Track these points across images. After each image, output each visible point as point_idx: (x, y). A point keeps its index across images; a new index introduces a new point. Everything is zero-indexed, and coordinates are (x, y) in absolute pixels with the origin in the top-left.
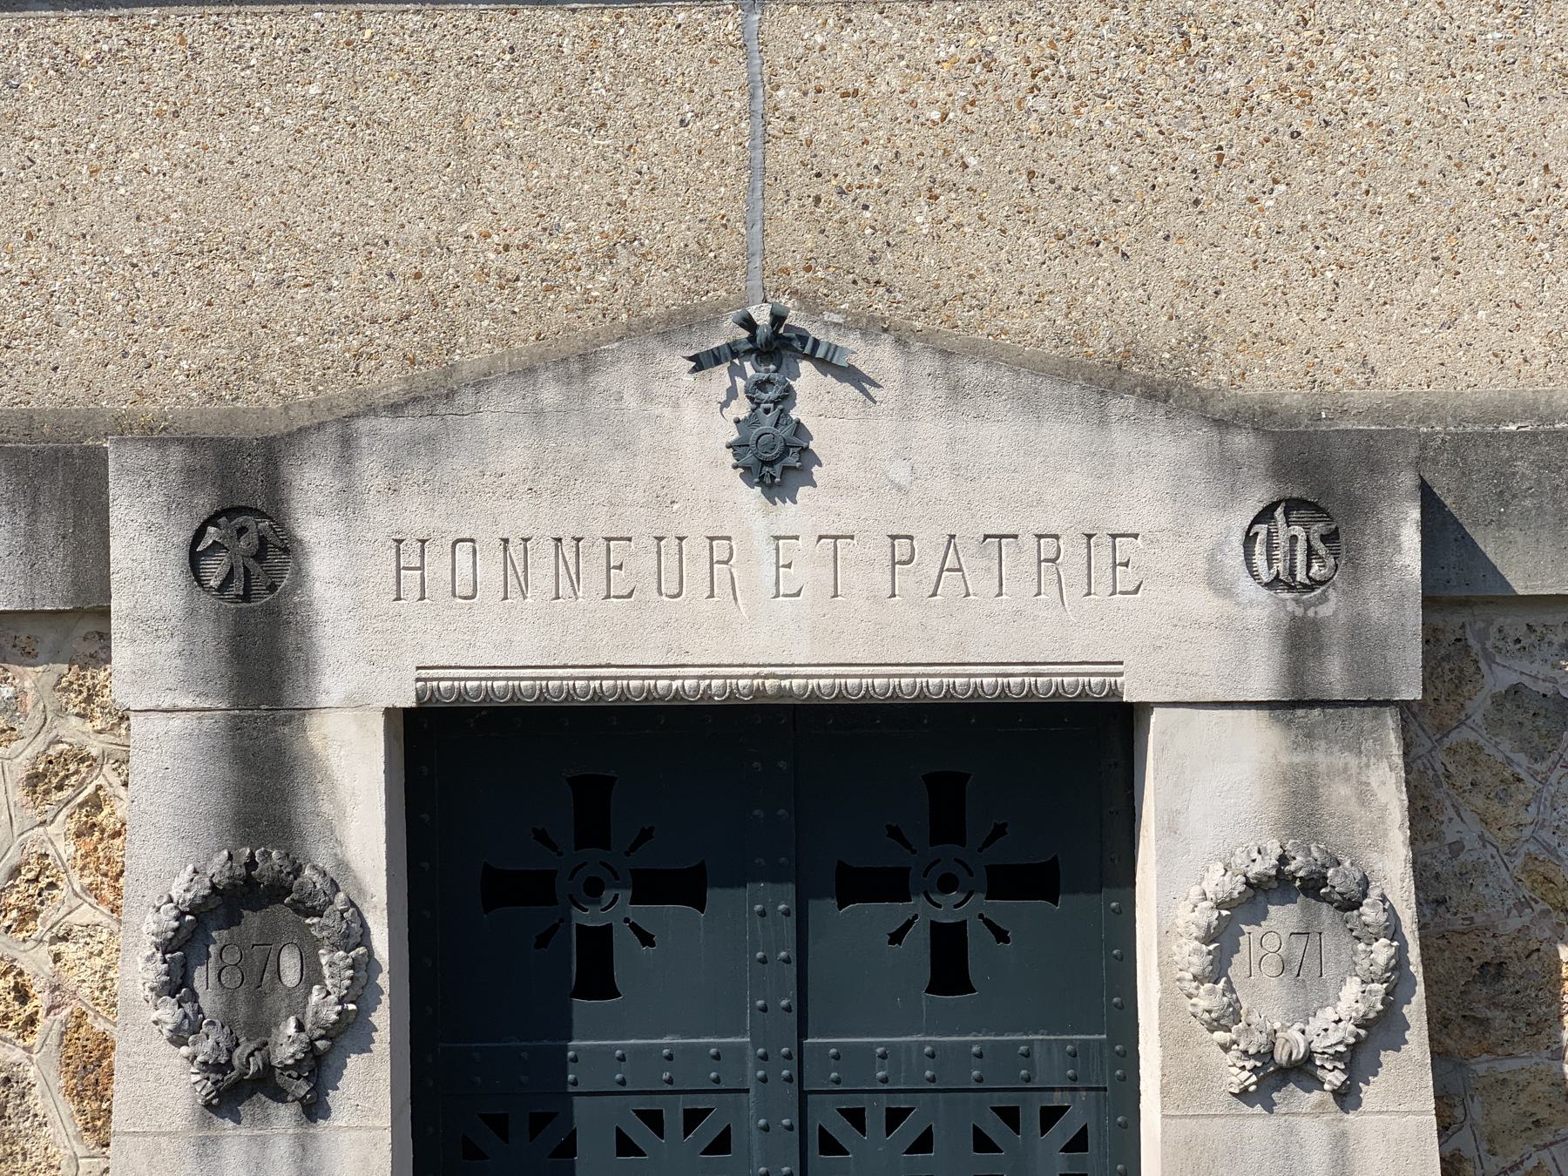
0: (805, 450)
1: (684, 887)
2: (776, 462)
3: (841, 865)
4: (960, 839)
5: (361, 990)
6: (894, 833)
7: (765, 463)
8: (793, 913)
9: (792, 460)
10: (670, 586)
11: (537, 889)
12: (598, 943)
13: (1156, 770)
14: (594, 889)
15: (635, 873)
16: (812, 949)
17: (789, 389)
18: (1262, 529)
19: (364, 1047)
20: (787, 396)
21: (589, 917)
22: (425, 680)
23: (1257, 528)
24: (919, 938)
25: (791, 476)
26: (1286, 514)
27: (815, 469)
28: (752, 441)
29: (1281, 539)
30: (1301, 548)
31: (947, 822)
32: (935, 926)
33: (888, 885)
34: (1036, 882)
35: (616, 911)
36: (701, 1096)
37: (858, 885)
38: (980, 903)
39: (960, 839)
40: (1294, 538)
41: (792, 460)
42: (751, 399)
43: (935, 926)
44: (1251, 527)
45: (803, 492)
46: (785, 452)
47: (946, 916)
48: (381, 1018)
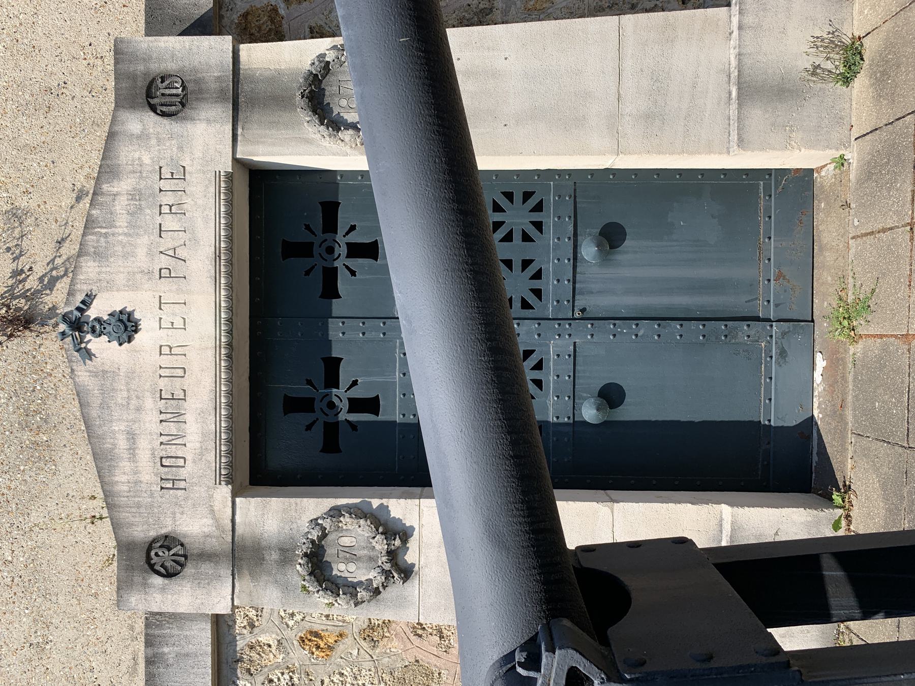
0: (121, 312)
1: (332, 366)
2: (125, 326)
3: (322, 296)
4: (311, 244)
5: (360, 513)
6: (308, 273)
7: (126, 329)
8: (749, 323)
9: (125, 318)
10: (180, 372)
11: (332, 430)
12: (356, 405)
13: (263, 155)
14: (332, 405)
15: (326, 387)
16: (597, 316)
17: (95, 319)
18: (159, 108)
19: (384, 508)
20: (98, 320)
21: (344, 405)
22: (220, 481)
23: (158, 112)
24: (353, 263)
25: (131, 319)
26: (153, 98)
27: (128, 310)
28: (117, 335)
29: (163, 100)
30: (167, 92)
31: (305, 250)
32: (348, 257)
33: (331, 275)
34: (330, 210)
35: (341, 395)
36: (173, 370)
37: (331, 292)
38: (339, 237)
39: (311, 244)
40: (163, 95)
41: (125, 318)
42: (100, 335)
43: (348, 257)
44: (158, 114)
45: (137, 315)
46: (120, 321)
47: (343, 250)
48: (375, 503)
